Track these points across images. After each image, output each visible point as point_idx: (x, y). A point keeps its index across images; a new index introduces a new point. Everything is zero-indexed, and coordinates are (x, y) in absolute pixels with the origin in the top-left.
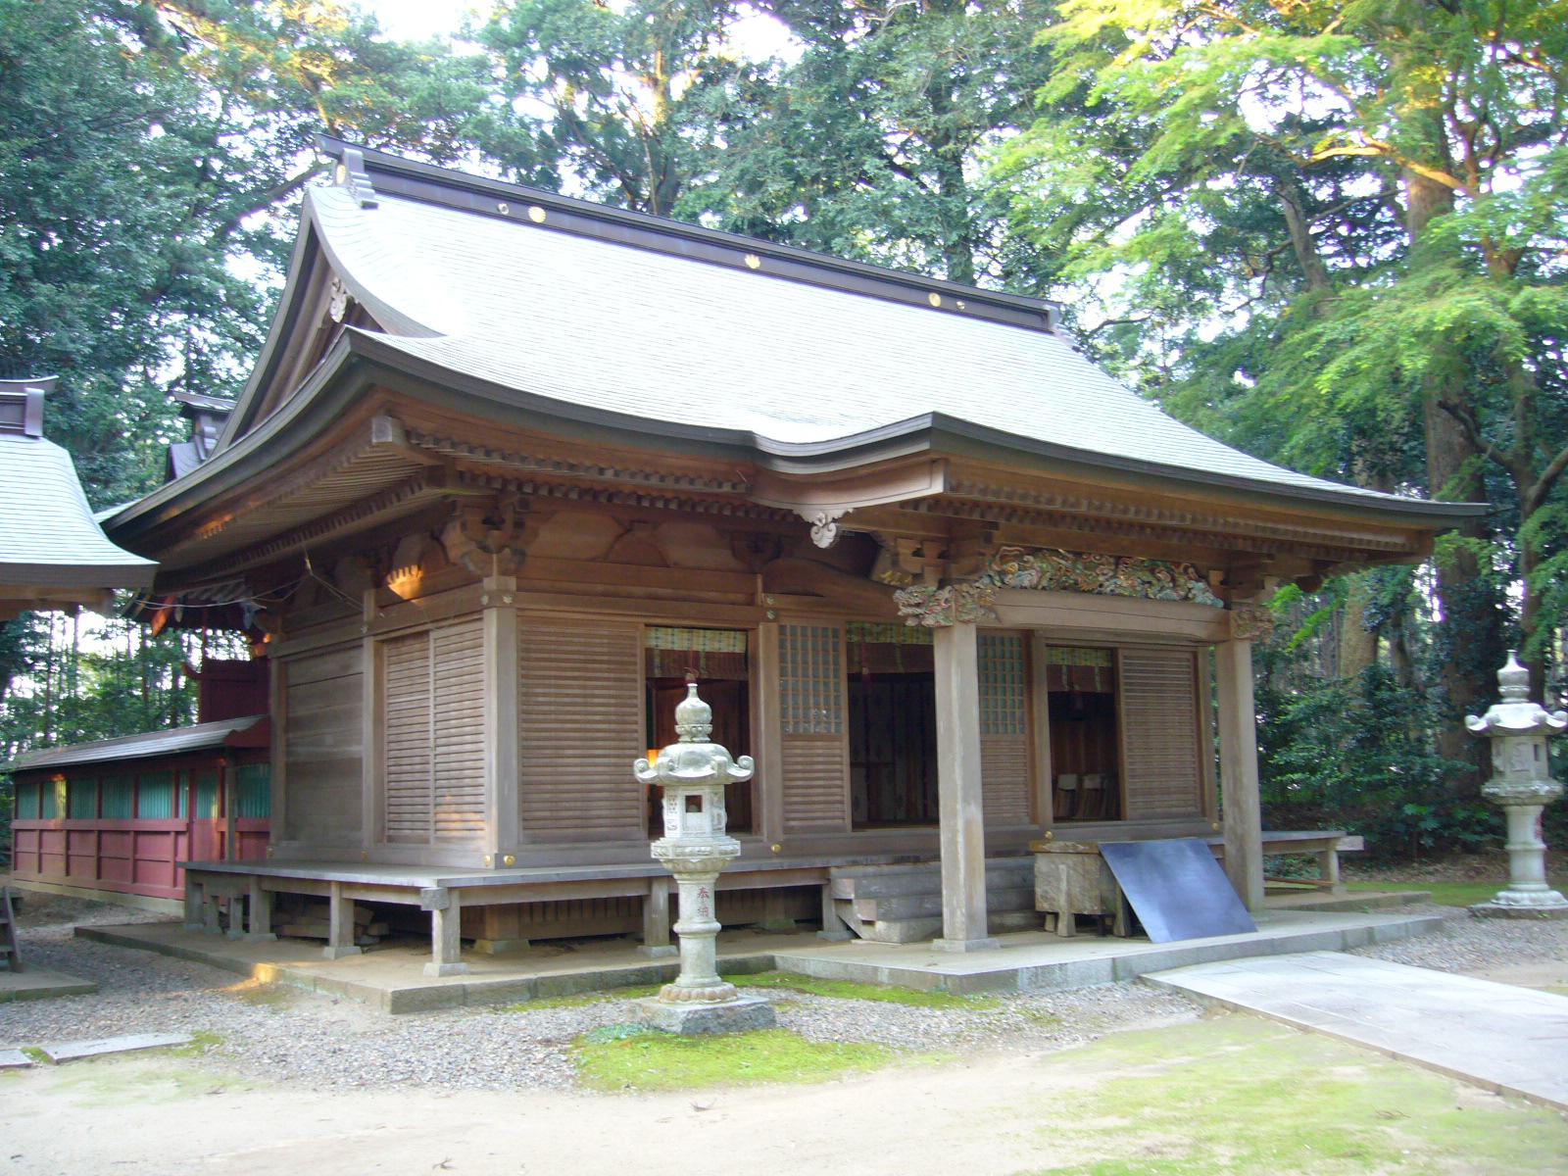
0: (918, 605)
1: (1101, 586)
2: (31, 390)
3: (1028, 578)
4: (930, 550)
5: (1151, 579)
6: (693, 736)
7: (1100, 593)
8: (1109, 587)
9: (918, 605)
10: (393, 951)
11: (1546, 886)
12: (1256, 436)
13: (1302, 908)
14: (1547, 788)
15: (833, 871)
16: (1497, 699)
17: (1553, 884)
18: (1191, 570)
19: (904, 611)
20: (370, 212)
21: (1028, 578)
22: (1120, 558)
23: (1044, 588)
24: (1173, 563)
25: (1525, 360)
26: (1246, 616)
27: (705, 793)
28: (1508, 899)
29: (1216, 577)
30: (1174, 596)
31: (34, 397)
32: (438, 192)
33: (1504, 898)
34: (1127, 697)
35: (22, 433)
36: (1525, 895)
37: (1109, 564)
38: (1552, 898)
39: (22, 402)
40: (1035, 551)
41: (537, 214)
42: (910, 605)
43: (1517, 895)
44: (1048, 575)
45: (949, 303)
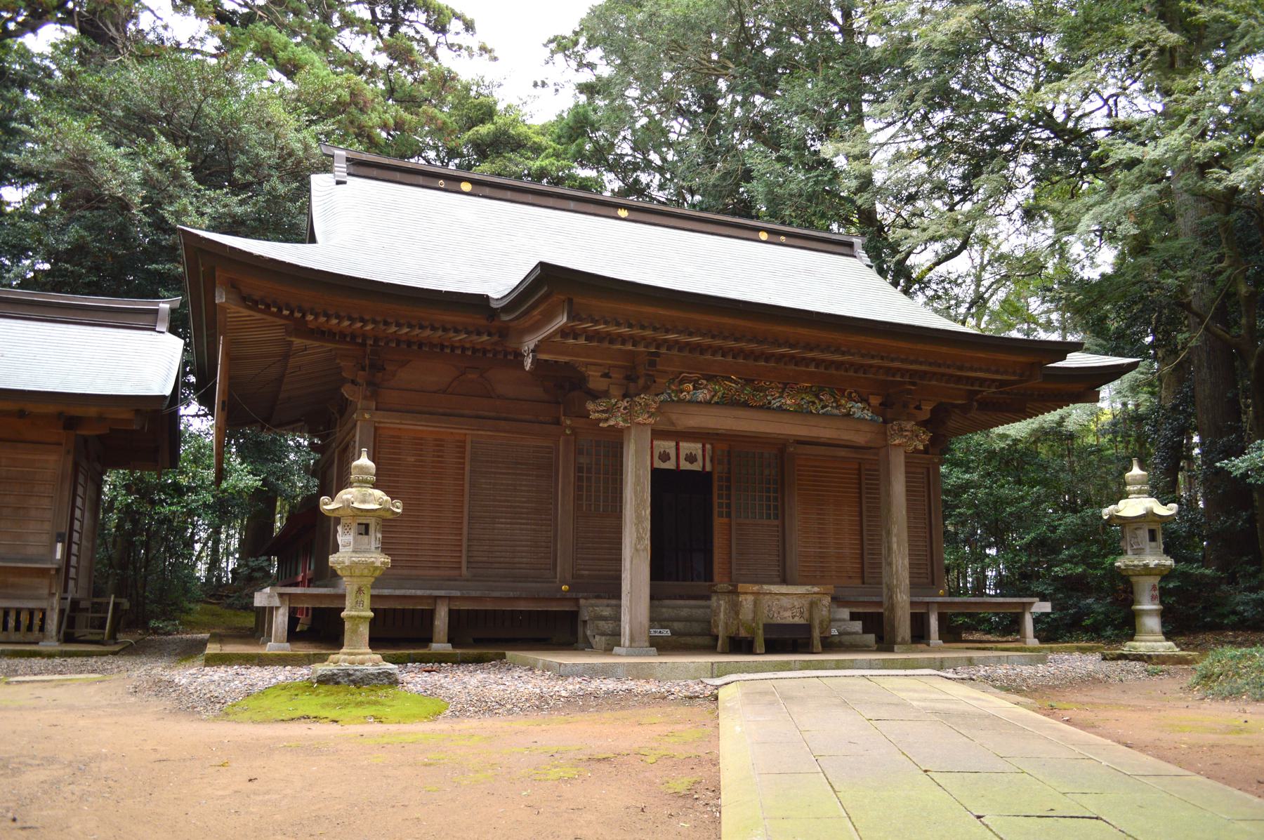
0: (603, 411)
1: (770, 403)
2: (161, 305)
3: (702, 395)
4: (616, 375)
5: (813, 399)
6: (363, 482)
7: (769, 408)
8: (776, 404)
9: (603, 411)
10: (234, 643)
11: (1162, 637)
12: (945, 312)
13: (967, 648)
14: (1157, 562)
15: (582, 602)
16: (1125, 495)
17: (1168, 635)
18: (854, 395)
19: (594, 416)
20: (340, 186)
21: (702, 395)
22: (785, 384)
23: (717, 403)
24: (839, 390)
25: (79, 68)
26: (896, 428)
27: (372, 522)
28: (1130, 647)
29: (875, 401)
30: (836, 412)
31: (164, 309)
32: (398, 176)
33: (1128, 647)
34: (868, 498)
35: (154, 330)
36: (1143, 644)
37: (778, 388)
38: (1164, 647)
39: (156, 312)
40: (710, 378)
41: (466, 187)
42: (598, 412)
43: (1137, 644)
44: (720, 394)
45: (774, 239)
